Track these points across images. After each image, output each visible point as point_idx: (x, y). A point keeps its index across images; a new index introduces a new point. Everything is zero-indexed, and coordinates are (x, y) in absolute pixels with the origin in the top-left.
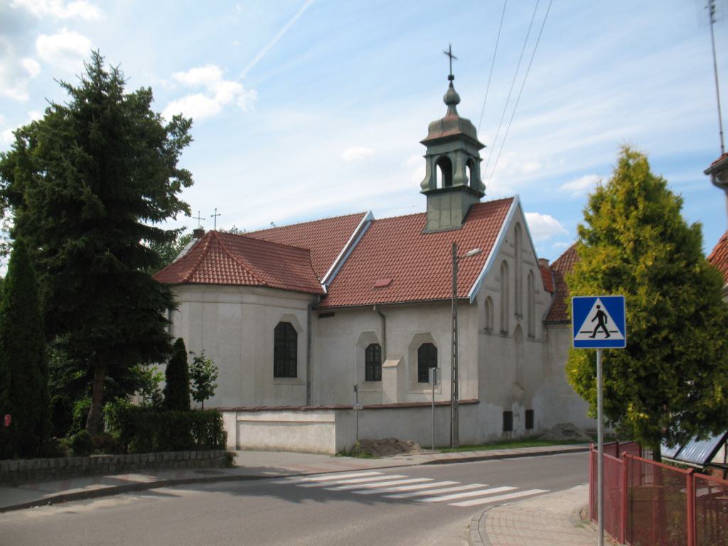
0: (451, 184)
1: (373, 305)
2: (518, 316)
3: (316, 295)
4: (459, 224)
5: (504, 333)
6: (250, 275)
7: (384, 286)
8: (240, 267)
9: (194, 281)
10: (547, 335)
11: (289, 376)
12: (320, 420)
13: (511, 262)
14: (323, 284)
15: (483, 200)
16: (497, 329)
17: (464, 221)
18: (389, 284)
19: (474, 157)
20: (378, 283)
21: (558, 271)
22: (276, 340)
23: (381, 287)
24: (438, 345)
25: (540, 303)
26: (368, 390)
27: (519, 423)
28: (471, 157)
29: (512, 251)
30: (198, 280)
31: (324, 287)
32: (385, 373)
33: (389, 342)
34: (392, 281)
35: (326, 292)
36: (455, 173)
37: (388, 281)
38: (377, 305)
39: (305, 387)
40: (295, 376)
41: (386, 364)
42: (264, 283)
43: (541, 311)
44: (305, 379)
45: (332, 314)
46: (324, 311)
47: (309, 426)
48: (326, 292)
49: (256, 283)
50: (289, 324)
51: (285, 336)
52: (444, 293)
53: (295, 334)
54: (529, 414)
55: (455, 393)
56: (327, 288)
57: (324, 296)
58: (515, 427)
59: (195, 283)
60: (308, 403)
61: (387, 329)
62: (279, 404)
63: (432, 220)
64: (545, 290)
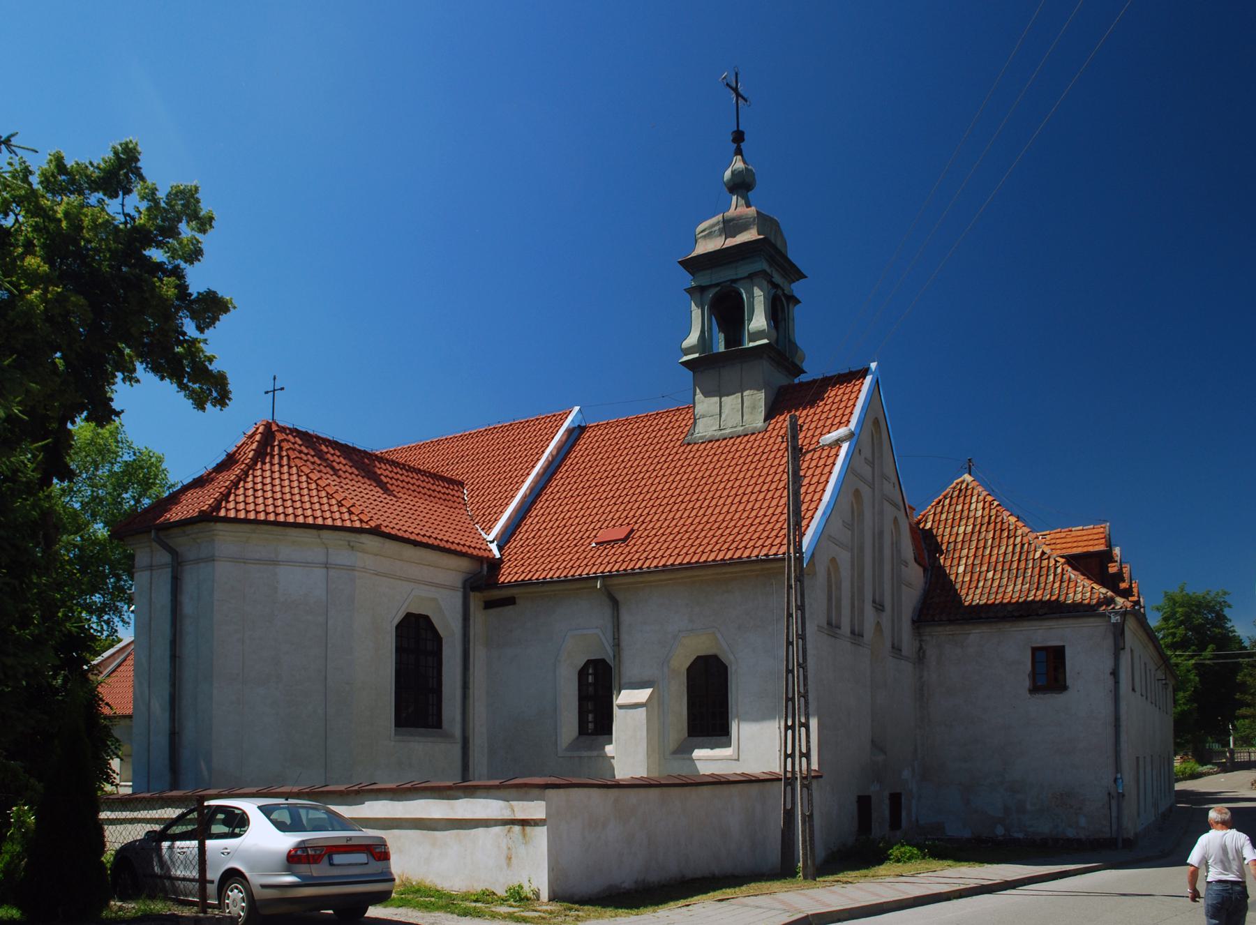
0: (741, 342)
1: (597, 578)
2: (879, 607)
3: (480, 560)
4: (759, 423)
5: (856, 635)
6: (345, 510)
7: (616, 541)
8: (323, 494)
9: (222, 513)
10: (921, 648)
11: (426, 726)
12: (507, 815)
13: (866, 491)
14: (492, 542)
15: (803, 378)
16: (846, 628)
17: (768, 417)
18: (624, 540)
19: (784, 295)
20: (603, 535)
21: (931, 529)
22: (399, 650)
23: (608, 542)
24: (732, 657)
25: (909, 585)
26: (585, 754)
27: (881, 810)
28: (780, 292)
29: (866, 471)
30: (232, 514)
31: (494, 547)
32: (620, 720)
33: (626, 655)
34: (632, 531)
35: (498, 555)
36: (750, 320)
37: (626, 530)
38: (604, 577)
39: (457, 749)
40: (438, 724)
41: (625, 697)
42: (373, 524)
43: (911, 597)
44: (458, 732)
45: (511, 601)
46: (496, 594)
47: (481, 831)
48: (498, 555)
49: (357, 524)
50: (426, 619)
51: (416, 640)
52: (745, 547)
53: (438, 640)
54: (896, 799)
55: (193, 880)
56: (500, 548)
57: (495, 565)
58: (904, 823)
59: (226, 520)
60: (465, 777)
61: (624, 629)
62: (411, 778)
63: (703, 416)
64: (916, 560)
